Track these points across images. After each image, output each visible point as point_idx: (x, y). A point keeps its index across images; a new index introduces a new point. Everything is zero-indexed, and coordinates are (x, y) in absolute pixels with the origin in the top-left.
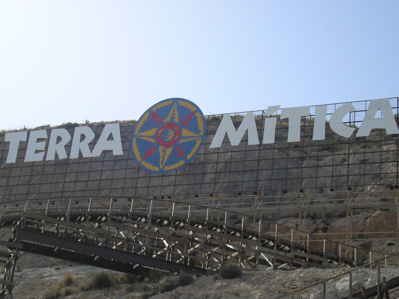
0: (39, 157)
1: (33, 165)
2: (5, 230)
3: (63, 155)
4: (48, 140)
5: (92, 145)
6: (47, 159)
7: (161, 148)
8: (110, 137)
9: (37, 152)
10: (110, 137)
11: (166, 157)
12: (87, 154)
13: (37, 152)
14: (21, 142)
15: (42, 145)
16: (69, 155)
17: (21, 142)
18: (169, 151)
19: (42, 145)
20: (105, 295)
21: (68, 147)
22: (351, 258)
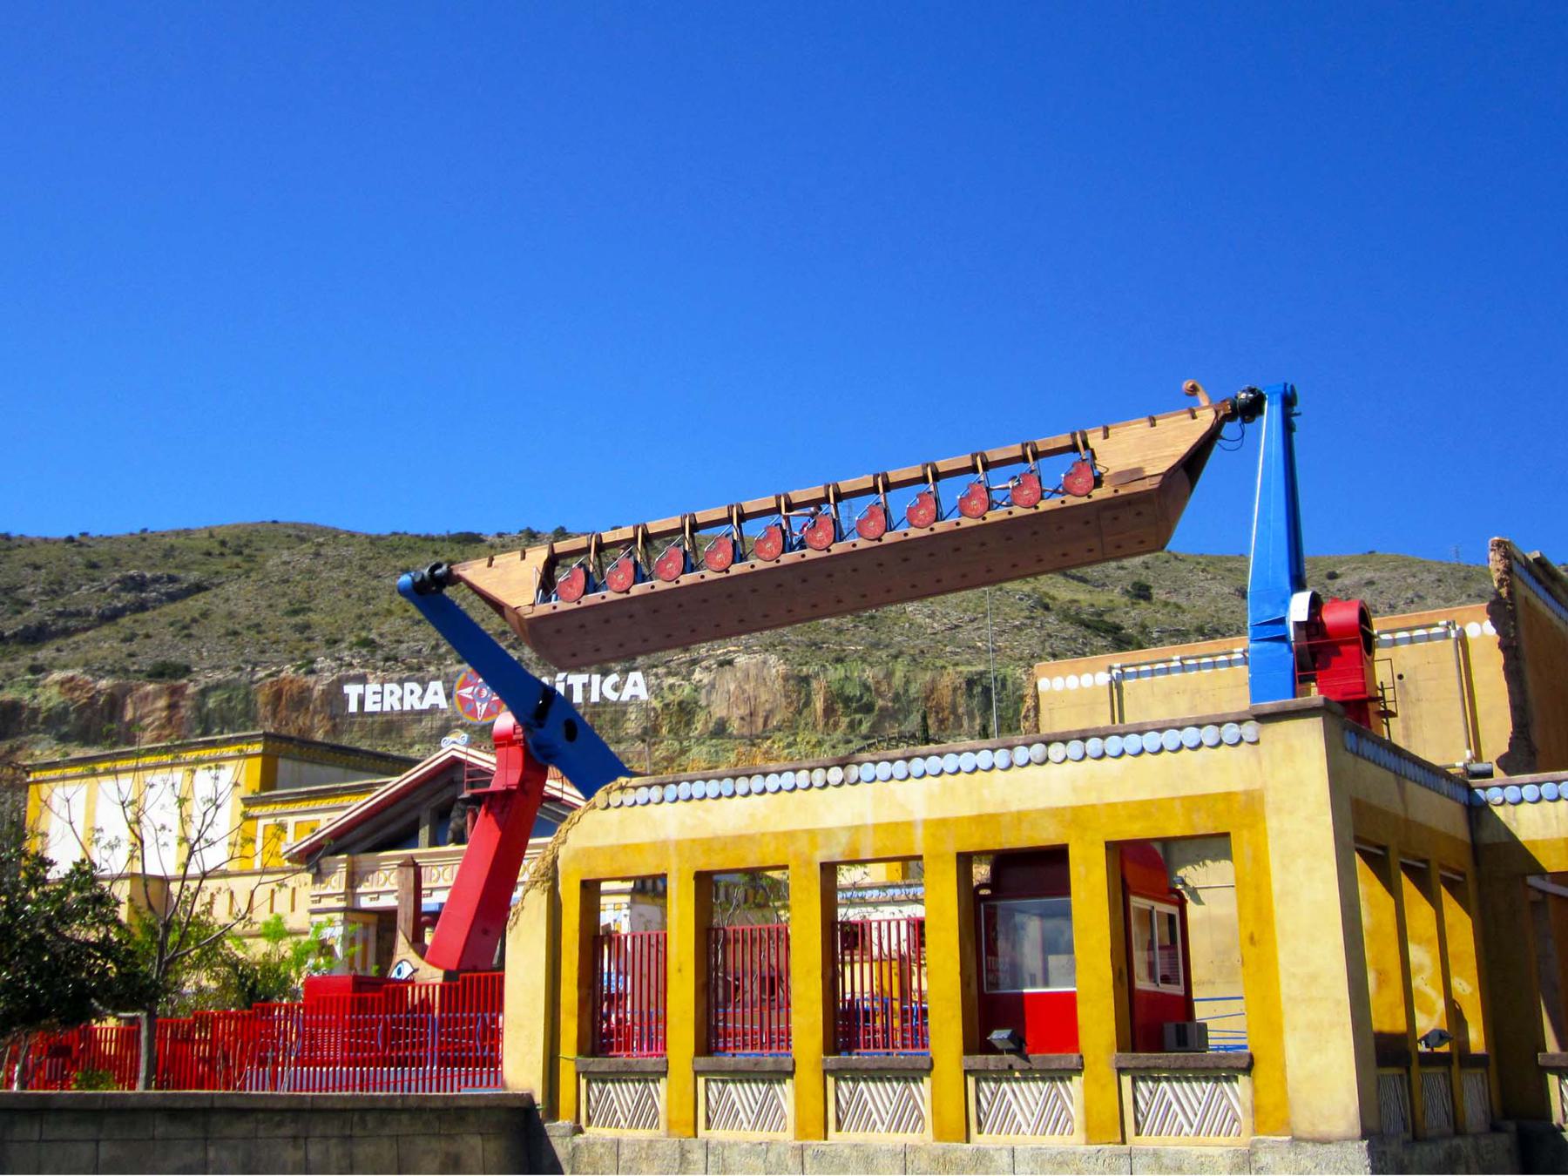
0: (377, 708)
1: (373, 714)
2: (771, 748)
3: (397, 707)
4: (382, 693)
5: (422, 698)
6: (622, 699)
7: (478, 704)
8: (436, 693)
9: (375, 703)
10: (635, 684)
11: (483, 711)
12: (418, 707)
13: (375, 703)
14: (359, 695)
15: (378, 698)
16: (402, 706)
17: (359, 695)
18: (485, 706)
19: (378, 698)
20: (269, 955)
21: (401, 699)
22: (594, 1085)
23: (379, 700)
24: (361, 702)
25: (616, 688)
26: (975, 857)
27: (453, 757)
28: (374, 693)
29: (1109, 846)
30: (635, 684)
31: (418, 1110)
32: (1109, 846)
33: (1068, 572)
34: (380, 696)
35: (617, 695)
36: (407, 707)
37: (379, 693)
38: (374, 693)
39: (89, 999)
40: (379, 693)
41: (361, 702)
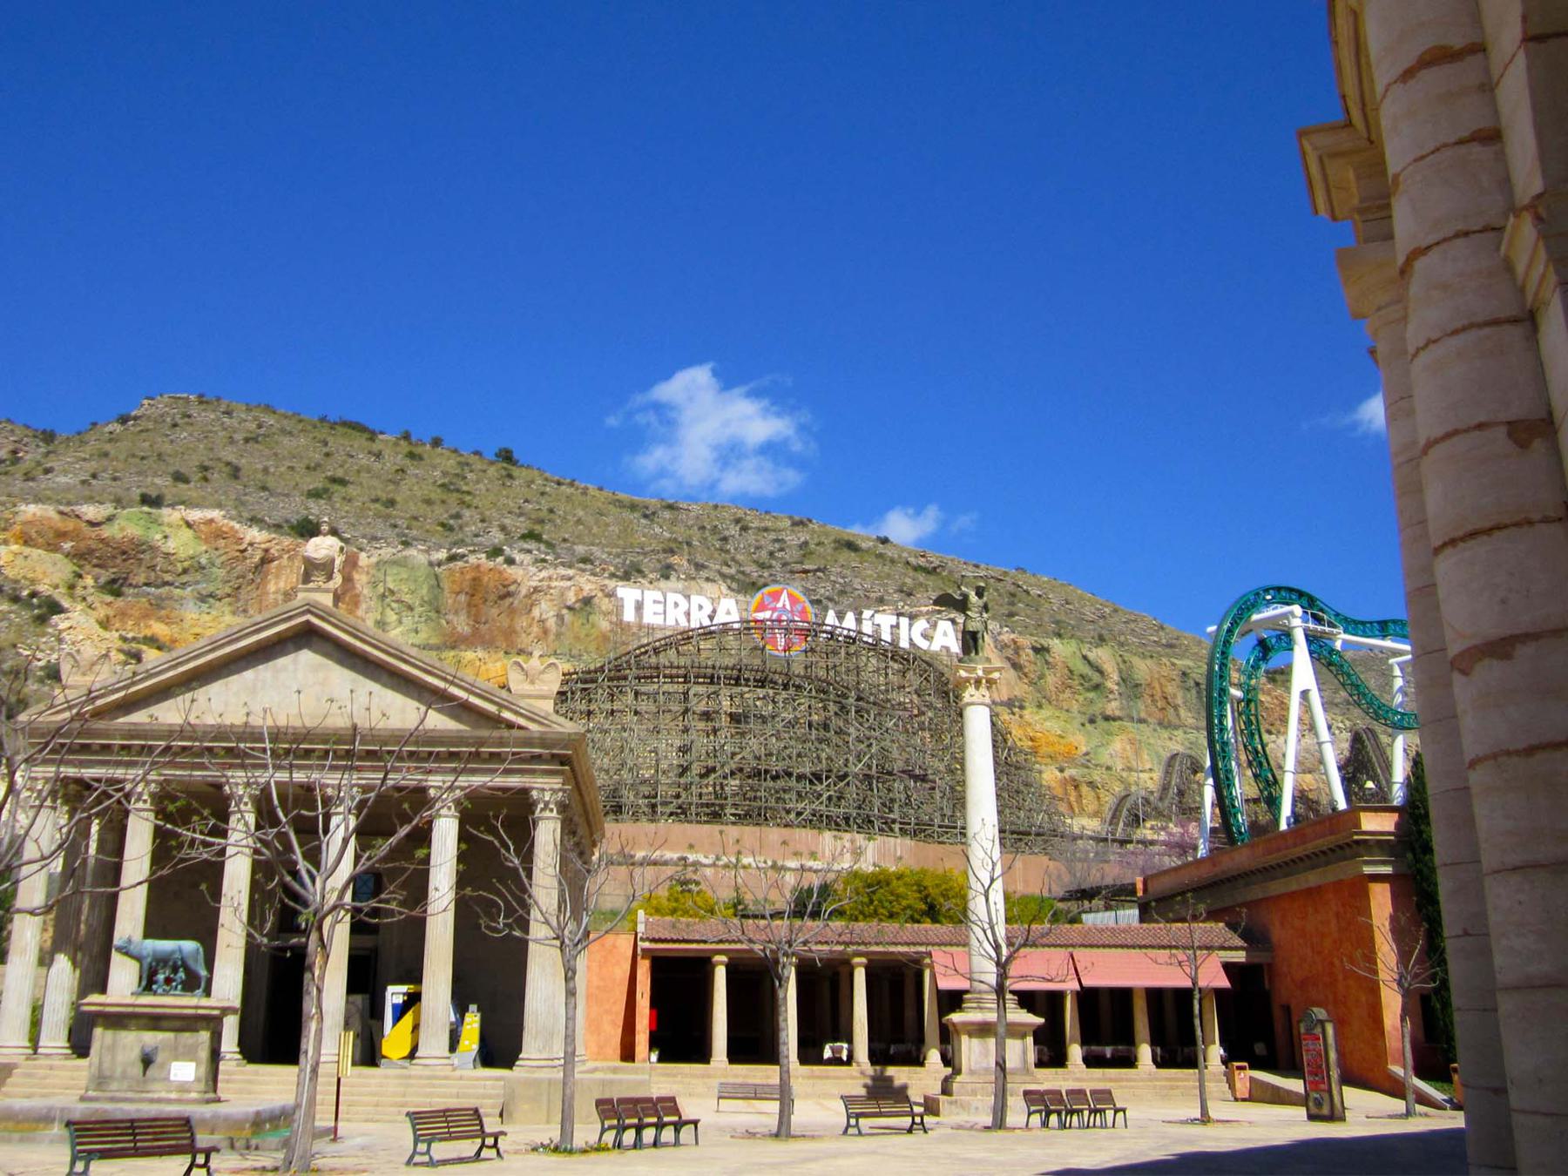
0: (658, 621)
10: (945, 634)
15: (660, 608)
17: (637, 602)
19: (660, 608)
21: (688, 614)
23: (661, 611)
24: (639, 607)
25: (926, 636)
26: (100, 1020)
27: (308, 622)
28: (655, 602)
29: (922, 1064)
30: (945, 634)
31: (1292, 896)
32: (922, 1064)
33: (1495, 80)
34: (661, 606)
35: (927, 643)
36: (695, 624)
37: (659, 602)
38: (655, 602)
39: (1283, 834)
40: (659, 602)
41: (639, 607)
